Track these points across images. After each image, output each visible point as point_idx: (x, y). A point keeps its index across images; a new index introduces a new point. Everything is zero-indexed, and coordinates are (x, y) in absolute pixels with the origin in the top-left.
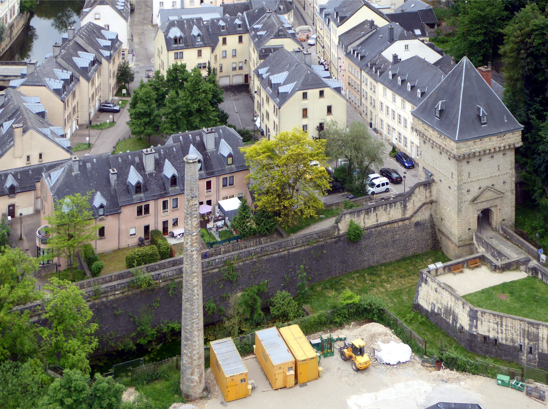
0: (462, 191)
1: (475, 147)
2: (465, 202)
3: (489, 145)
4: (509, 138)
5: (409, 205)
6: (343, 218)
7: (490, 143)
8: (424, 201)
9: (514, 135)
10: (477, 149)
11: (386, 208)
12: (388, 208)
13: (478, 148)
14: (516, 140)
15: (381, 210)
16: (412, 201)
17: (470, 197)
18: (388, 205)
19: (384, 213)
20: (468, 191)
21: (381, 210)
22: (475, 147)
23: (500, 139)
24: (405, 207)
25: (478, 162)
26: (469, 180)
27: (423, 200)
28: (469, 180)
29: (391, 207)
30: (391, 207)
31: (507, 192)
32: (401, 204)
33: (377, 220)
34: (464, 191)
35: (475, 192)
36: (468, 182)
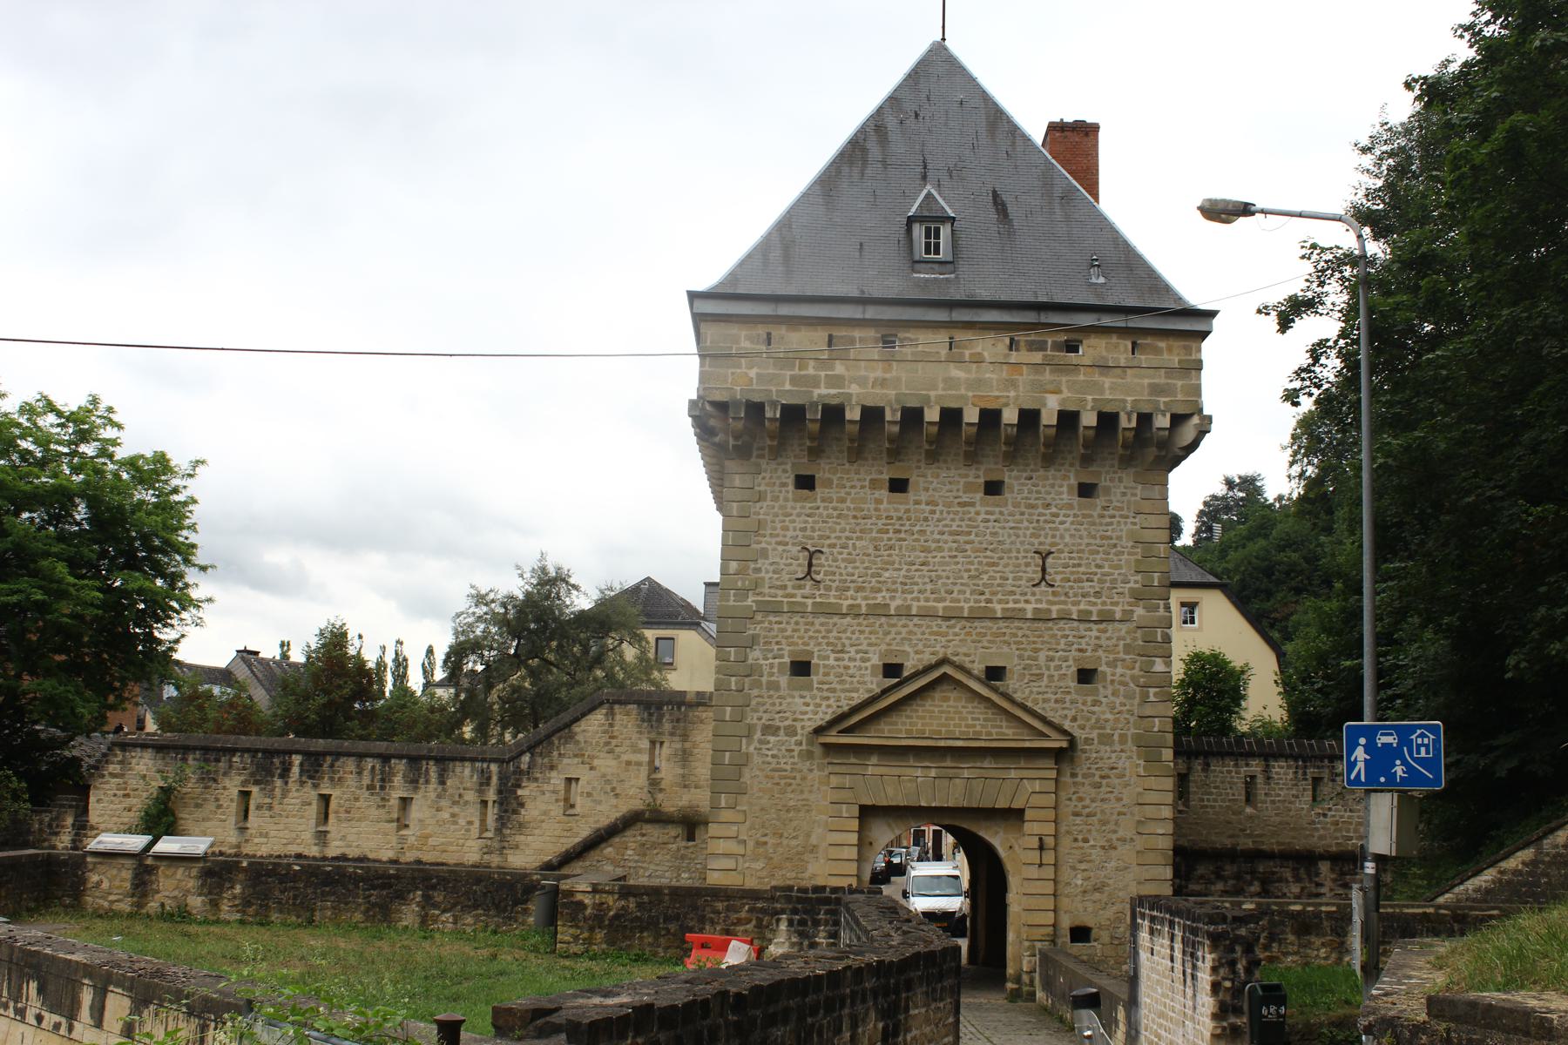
0: (754, 655)
1: (839, 369)
2: (770, 729)
3: (950, 382)
4: (1104, 368)
5: (538, 800)
6: (114, 768)
7: (956, 372)
8: (637, 805)
9: (1143, 359)
10: (854, 389)
11: (385, 780)
12: (398, 780)
13: (862, 382)
14: (1156, 390)
15: (351, 780)
16: (557, 780)
17: (810, 708)
18: (400, 766)
19: (367, 802)
20: (801, 668)
21: (351, 780)
22: (839, 369)
23: (1037, 357)
24: (509, 803)
25: (884, 493)
26: (806, 595)
27: (634, 797)
28: (806, 595)
29: (413, 782)
30: (413, 782)
31: (1106, 739)
32: (485, 781)
33: (322, 837)
34: (771, 662)
35: (851, 677)
36: (796, 610)
